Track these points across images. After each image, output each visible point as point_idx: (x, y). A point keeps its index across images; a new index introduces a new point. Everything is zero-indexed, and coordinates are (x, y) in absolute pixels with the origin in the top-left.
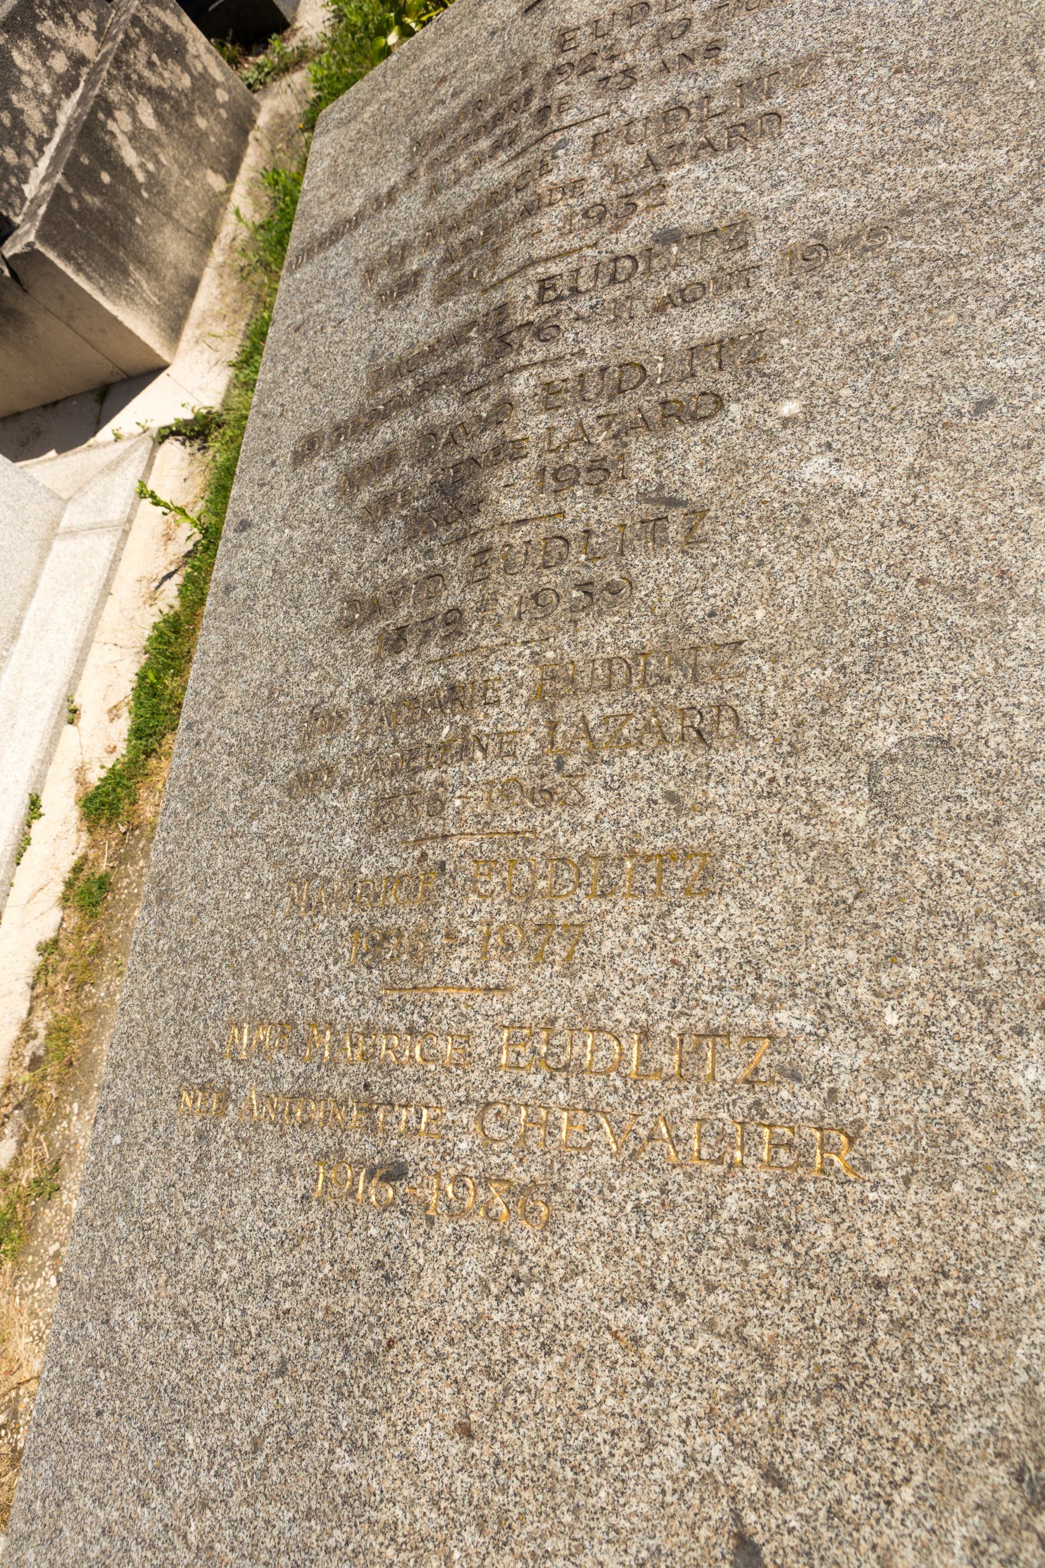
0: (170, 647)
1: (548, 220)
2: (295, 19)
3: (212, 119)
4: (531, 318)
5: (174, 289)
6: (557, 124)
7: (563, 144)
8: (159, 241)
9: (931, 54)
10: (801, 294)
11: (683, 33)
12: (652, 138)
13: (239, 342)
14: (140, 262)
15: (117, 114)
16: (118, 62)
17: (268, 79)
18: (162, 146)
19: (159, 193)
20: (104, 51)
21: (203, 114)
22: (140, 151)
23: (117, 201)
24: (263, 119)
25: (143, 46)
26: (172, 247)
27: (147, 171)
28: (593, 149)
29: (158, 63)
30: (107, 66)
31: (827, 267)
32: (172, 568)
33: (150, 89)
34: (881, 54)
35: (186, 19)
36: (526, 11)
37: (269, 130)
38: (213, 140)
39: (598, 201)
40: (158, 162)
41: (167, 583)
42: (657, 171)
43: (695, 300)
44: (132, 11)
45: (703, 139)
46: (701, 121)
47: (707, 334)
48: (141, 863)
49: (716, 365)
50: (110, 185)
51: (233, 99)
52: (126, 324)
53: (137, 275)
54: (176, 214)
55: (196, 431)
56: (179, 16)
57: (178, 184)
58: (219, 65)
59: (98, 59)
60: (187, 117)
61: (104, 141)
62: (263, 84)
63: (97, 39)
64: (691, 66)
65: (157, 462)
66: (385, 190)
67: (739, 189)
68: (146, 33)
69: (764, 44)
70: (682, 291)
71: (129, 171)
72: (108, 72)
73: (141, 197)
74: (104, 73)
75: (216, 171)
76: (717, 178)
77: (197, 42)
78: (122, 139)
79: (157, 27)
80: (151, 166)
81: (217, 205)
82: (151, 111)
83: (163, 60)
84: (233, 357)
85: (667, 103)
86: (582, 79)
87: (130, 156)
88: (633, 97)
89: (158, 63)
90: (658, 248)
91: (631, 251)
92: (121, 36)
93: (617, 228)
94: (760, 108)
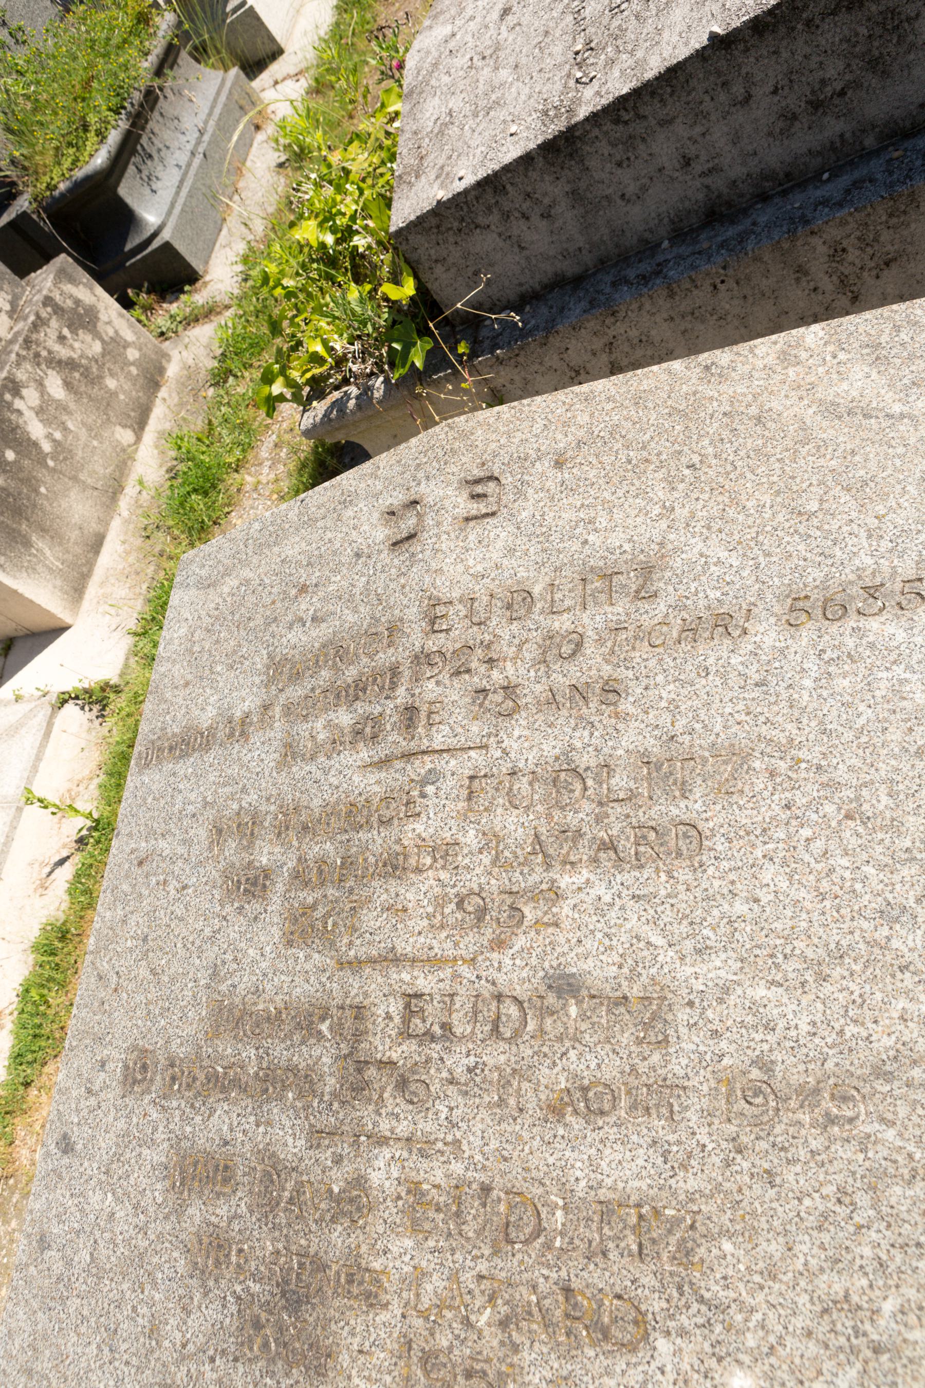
0: (58, 949)
1: (417, 892)
2: (206, 272)
3: (122, 379)
4: (395, 1056)
5: (78, 550)
6: (426, 742)
7: (432, 777)
8: (64, 505)
9: (891, 802)
10: (746, 1165)
11: (574, 654)
12: (539, 808)
13: (139, 608)
14: (43, 530)
15: (24, 392)
16: (27, 342)
17: (180, 328)
18: (70, 413)
19: (65, 459)
20: (16, 329)
21: (112, 375)
22: (46, 422)
23: (21, 475)
24: (173, 370)
25: (54, 323)
26: (76, 508)
27: (54, 441)
28: (469, 799)
29: (69, 335)
30: (16, 347)
31: (778, 1129)
32: (65, 854)
33: (60, 362)
34: (824, 779)
35: (99, 290)
36: (394, 544)
37: (177, 381)
38: (122, 397)
39: (476, 889)
40: (66, 429)
41: (58, 871)
42: (548, 866)
43: (602, 1113)
44: (45, 292)
45: (602, 834)
46: (601, 804)
47: (621, 1185)
48: (14, 1224)
49: (634, 1247)
50: (15, 462)
51: (143, 355)
52: (27, 595)
53: (39, 543)
54: (82, 476)
55: (96, 699)
56: (91, 289)
57: (86, 446)
58: (131, 326)
59: (9, 336)
60: (94, 380)
61: (10, 420)
62: (176, 332)
63: (11, 317)
64: (584, 710)
65: (56, 729)
66: (238, 714)
67: (653, 939)
68: (58, 310)
69: (673, 707)
70: (585, 1090)
71: (36, 444)
72: (18, 355)
73: (46, 466)
74: (13, 356)
75: (124, 426)
76: (622, 908)
77: (106, 305)
78: (29, 415)
79: (69, 303)
80: (58, 435)
81: (123, 461)
82: (60, 382)
83: (74, 332)
84: (132, 624)
85: (557, 758)
86: (456, 681)
87: (36, 429)
88: (516, 733)
89: (69, 335)
90: (551, 999)
91: (518, 991)
92: (32, 318)
93: (499, 944)
94: (675, 811)
